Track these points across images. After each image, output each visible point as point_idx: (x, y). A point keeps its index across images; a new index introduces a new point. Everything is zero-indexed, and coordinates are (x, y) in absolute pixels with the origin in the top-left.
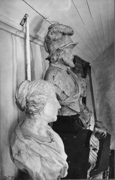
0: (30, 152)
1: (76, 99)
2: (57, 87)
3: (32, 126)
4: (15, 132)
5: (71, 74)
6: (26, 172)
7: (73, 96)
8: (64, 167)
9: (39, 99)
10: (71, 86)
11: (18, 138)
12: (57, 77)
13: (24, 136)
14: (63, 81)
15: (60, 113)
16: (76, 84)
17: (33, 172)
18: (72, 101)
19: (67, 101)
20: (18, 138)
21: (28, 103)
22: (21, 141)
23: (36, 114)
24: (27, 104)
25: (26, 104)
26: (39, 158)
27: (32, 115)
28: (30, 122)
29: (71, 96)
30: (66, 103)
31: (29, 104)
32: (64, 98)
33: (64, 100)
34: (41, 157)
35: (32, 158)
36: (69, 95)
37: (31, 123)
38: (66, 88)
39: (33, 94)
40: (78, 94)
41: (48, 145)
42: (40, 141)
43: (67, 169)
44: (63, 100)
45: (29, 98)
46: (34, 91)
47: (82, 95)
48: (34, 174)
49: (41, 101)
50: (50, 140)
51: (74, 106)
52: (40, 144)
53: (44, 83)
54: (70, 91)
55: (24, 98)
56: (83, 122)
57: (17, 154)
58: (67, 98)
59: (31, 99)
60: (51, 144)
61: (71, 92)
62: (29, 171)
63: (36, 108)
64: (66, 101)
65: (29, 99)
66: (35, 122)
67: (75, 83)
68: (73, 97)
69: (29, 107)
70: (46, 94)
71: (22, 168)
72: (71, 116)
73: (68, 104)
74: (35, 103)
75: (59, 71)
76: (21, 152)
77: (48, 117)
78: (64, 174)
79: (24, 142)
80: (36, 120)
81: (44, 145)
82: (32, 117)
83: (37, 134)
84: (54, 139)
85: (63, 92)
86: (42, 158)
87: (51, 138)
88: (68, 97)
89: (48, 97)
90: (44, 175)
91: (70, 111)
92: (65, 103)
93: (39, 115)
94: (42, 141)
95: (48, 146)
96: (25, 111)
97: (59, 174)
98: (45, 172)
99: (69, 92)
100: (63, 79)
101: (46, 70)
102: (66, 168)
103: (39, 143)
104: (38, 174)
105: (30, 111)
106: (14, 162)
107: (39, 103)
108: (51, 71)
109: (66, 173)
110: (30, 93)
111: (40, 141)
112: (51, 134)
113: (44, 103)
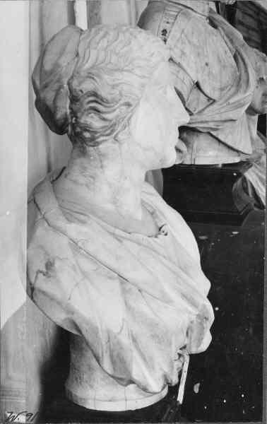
0: (87, 266)
1: (239, 110)
2: (175, 68)
3: (92, 180)
4: (35, 202)
5: (223, 28)
6: (74, 332)
7: (229, 98)
8: (198, 316)
9: (114, 87)
10: (224, 67)
11: (47, 221)
12: (174, 33)
13: (64, 214)
14: (194, 45)
15: (185, 157)
16: (240, 60)
17: (97, 328)
18: (224, 117)
19: (211, 116)
20: (44, 218)
21: (78, 100)
22: (56, 229)
23: (106, 140)
24: (74, 106)
25: (71, 108)
26: (116, 284)
27: (91, 144)
28: (85, 168)
29: (223, 99)
30: (207, 122)
31: (82, 105)
32: (198, 104)
33: (200, 112)
34: (123, 280)
35: (92, 283)
36: (215, 95)
37: (90, 172)
38: (206, 72)
39: (94, 71)
40: (245, 92)
41: (145, 243)
42: (120, 228)
43: (209, 324)
44: (196, 112)
45: (80, 83)
46: (97, 59)
47: (258, 106)
48: (100, 333)
49: (121, 94)
50: (153, 231)
51: (231, 133)
52: (119, 240)
53: (131, 34)
54: (221, 82)
55: (61, 87)
56: (260, 192)
57: (44, 270)
58: (212, 104)
59: (88, 86)
60: (156, 239)
61: (223, 86)
62: (84, 328)
63: (104, 119)
64: (204, 117)
65: (81, 88)
66: (102, 167)
67: (235, 57)
68: (229, 104)
69: (79, 115)
70: (137, 71)
71: (60, 318)
72: (224, 165)
73: (212, 125)
74: (102, 100)
75: (184, 14)
76: (57, 264)
77: (145, 149)
78: (200, 340)
79: (64, 233)
80: (105, 163)
81: (134, 242)
82: (91, 149)
83: (110, 207)
84: (166, 226)
85: (197, 85)
86: (128, 286)
87: (156, 223)
88: (212, 101)
89: (143, 81)
90: (134, 340)
91: (219, 150)
92: (202, 122)
93: (116, 146)
94: (125, 231)
95: (147, 247)
96: (67, 131)
97: (183, 340)
98: (136, 329)
99: (218, 85)
100: (195, 41)
101: (140, 14)
102: (207, 319)
103: (119, 239)
104: (115, 337)
105: (86, 130)
106: (32, 298)
107: (113, 99)
108: (157, 14)
109: (207, 339)
110: (80, 67)
111: (120, 228)
112: (158, 213)
113: (133, 99)
